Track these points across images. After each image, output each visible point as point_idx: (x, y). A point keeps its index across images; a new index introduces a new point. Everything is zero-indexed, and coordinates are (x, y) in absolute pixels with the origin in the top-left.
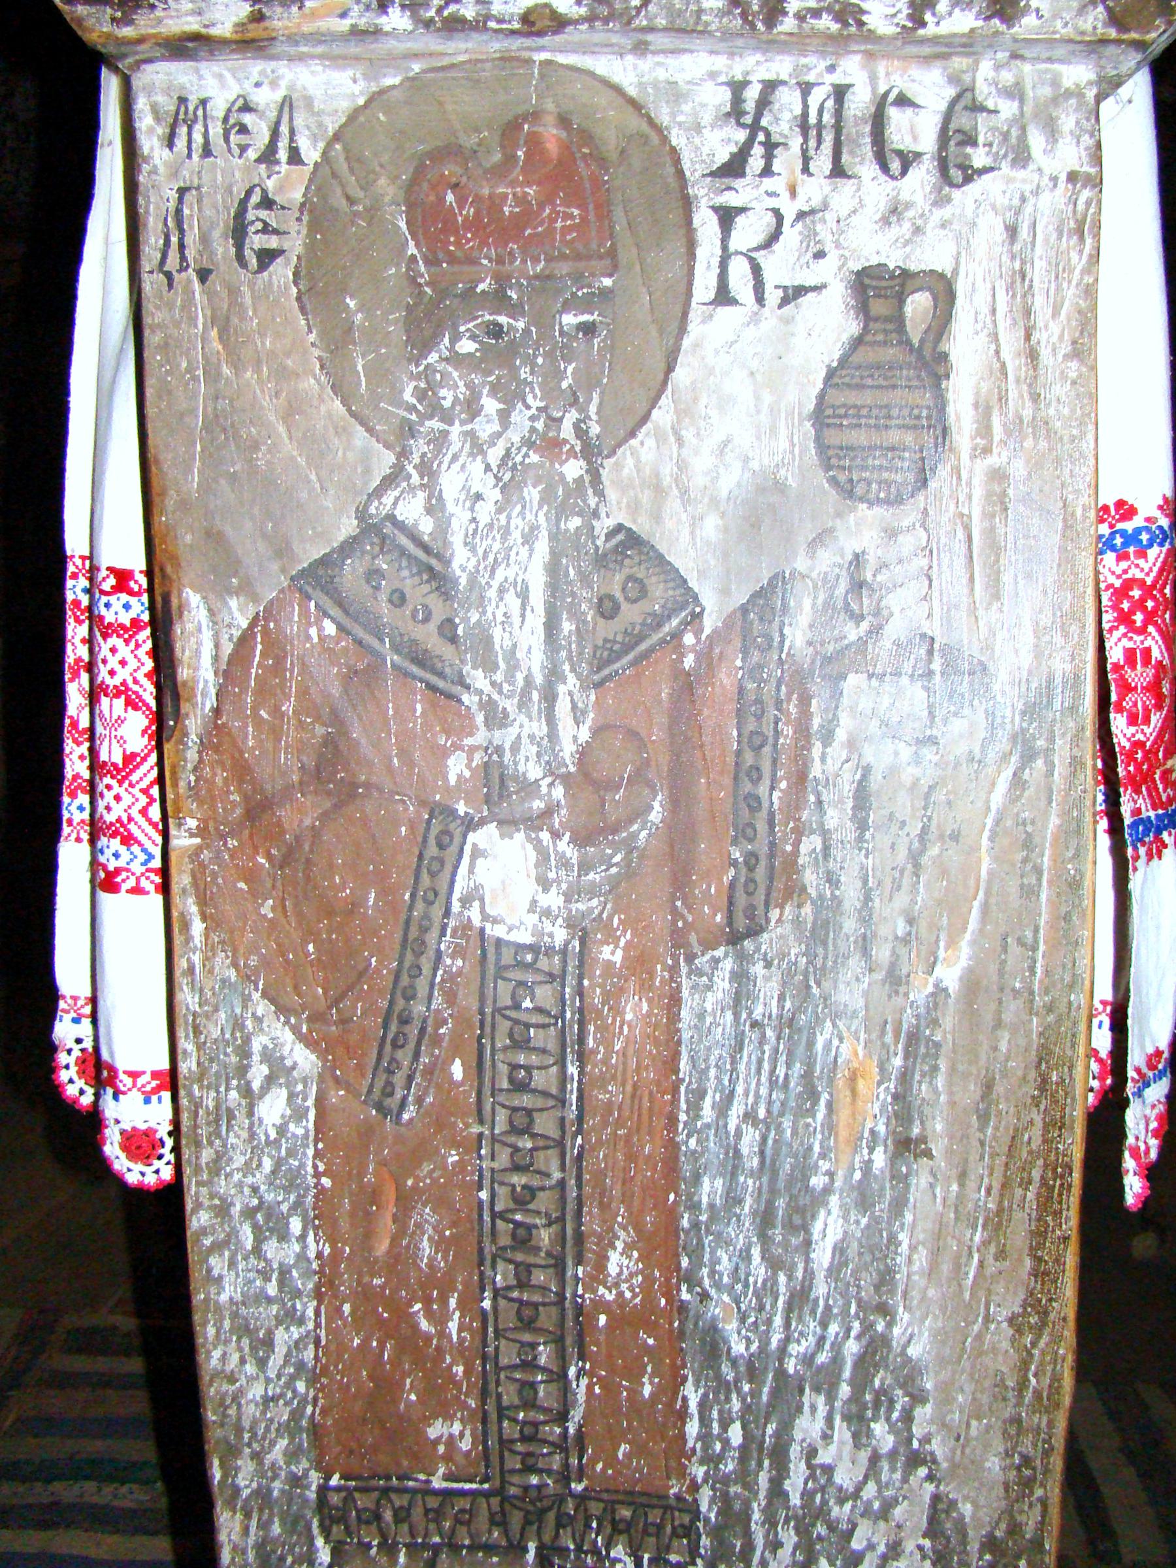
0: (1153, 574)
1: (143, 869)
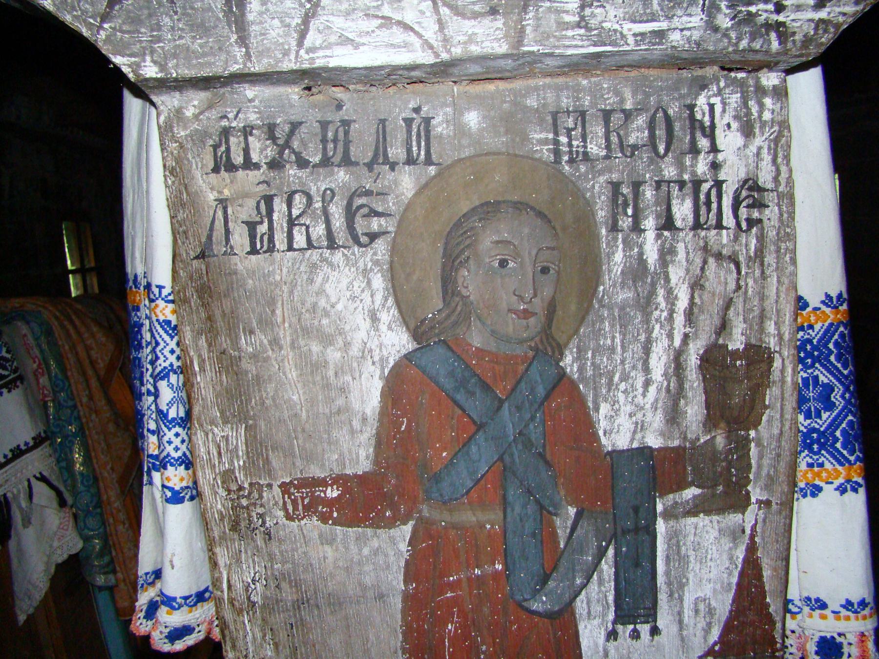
0: (824, 426)
1: (157, 302)
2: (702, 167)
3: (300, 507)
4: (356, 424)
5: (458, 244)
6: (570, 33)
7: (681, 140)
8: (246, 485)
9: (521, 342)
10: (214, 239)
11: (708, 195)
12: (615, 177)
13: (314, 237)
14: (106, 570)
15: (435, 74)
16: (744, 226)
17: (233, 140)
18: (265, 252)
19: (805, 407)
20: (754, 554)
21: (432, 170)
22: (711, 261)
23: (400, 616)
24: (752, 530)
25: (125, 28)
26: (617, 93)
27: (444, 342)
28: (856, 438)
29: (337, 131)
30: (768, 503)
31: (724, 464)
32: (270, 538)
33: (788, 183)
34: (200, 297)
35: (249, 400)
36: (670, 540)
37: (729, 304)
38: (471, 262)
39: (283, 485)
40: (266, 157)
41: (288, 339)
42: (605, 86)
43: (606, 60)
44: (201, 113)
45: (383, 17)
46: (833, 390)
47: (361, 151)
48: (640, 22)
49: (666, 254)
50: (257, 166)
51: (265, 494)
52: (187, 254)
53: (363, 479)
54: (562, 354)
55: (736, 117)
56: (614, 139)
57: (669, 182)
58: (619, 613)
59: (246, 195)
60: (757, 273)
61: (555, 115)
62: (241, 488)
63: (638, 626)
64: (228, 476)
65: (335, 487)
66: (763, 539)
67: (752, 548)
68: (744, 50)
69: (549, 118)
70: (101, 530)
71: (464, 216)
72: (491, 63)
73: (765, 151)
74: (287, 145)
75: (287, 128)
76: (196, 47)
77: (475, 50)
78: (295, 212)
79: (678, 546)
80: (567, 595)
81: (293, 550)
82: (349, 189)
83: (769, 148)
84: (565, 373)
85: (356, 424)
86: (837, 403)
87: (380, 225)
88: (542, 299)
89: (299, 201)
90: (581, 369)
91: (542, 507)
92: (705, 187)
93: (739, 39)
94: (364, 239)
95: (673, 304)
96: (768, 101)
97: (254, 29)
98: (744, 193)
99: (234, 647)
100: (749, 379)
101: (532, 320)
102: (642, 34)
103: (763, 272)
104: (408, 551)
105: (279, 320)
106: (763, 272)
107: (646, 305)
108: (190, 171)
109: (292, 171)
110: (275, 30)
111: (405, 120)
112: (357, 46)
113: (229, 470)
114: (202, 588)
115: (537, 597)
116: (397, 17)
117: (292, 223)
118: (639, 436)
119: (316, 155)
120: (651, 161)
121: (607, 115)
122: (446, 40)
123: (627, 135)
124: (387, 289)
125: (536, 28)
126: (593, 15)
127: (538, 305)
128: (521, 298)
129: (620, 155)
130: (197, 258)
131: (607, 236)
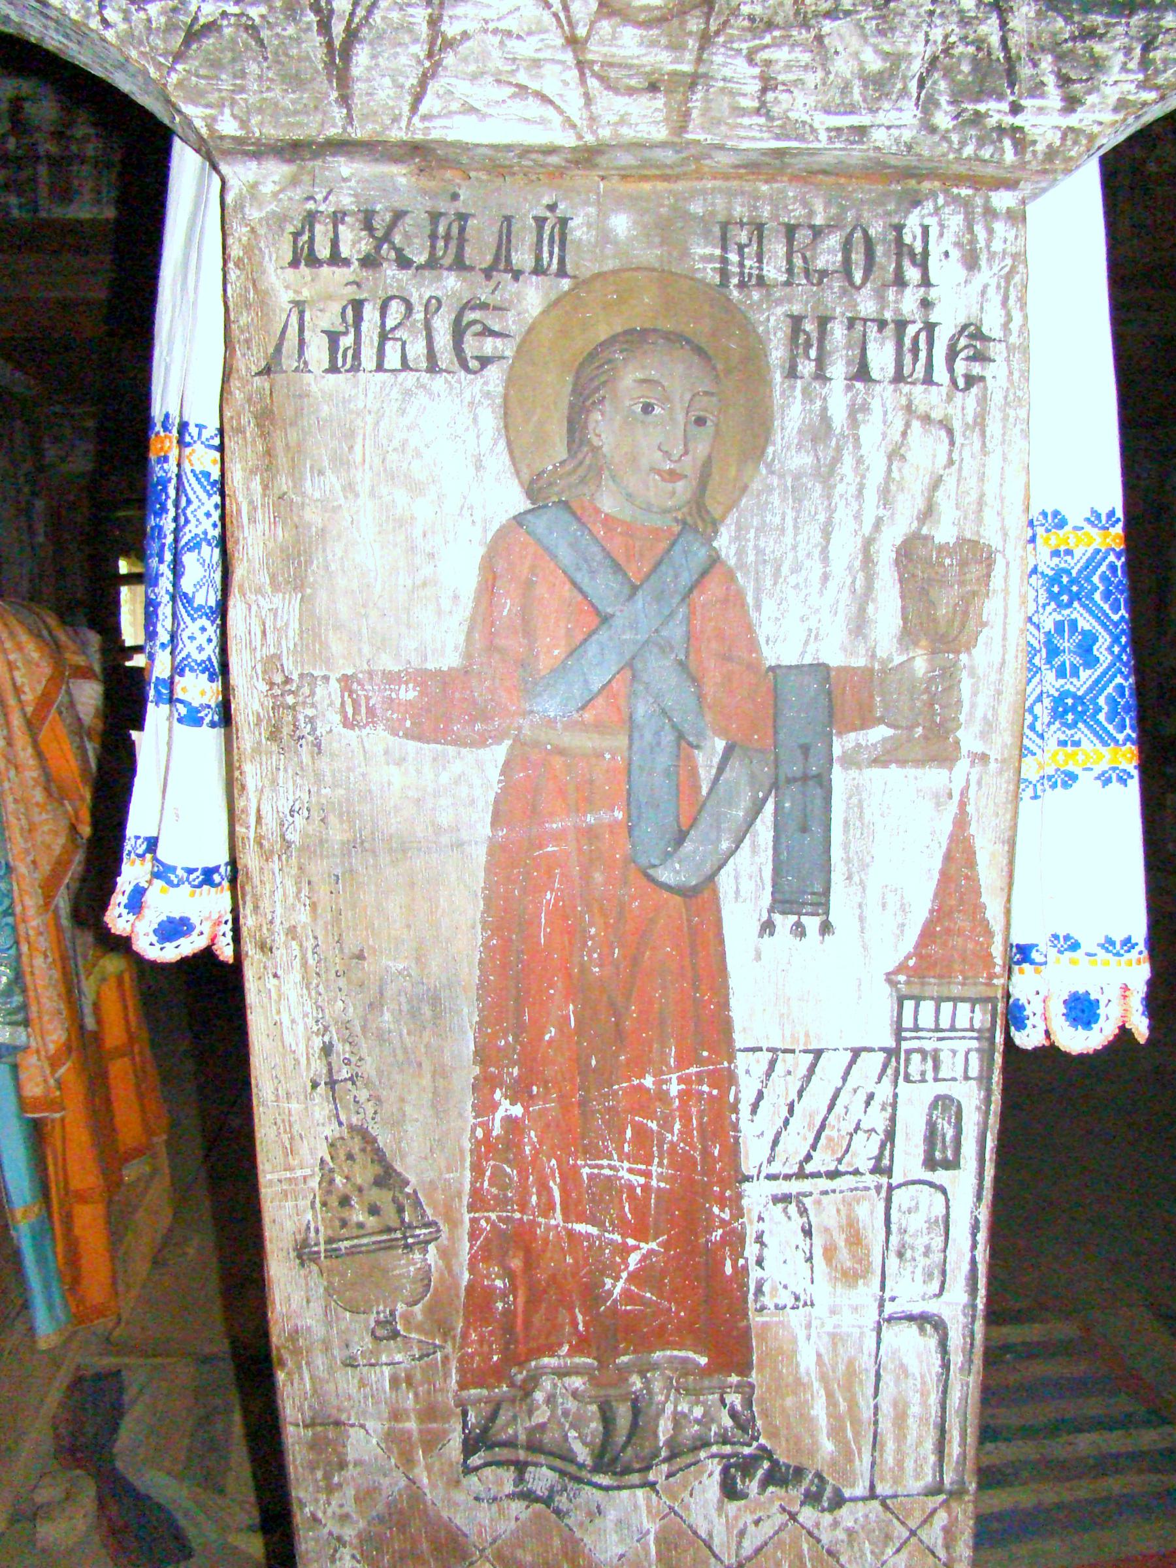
2: (909, 303)
3: (363, 710)
4: (446, 604)
5: (592, 380)
6: (746, 121)
7: (883, 268)
8: (295, 677)
9: (665, 511)
10: (284, 350)
11: (916, 339)
12: (796, 309)
13: (411, 356)
14: (14, 1018)
15: (577, 163)
16: (961, 383)
17: (318, 228)
18: (348, 371)
19: (1057, 662)
20: (964, 830)
21: (566, 284)
22: (916, 424)
23: (482, 874)
24: (962, 794)
25: (202, 72)
26: (805, 204)
27: (566, 503)
28: (1127, 709)
29: (450, 225)
30: (984, 758)
31: (925, 697)
32: (319, 753)
33: (1020, 333)
34: (258, 425)
35: (309, 562)
36: (850, 798)
37: (936, 483)
38: (607, 403)
39: (346, 680)
40: (359, 252)
41: (368, 483)
42: (791, 194)
43: (793, 161)
44: (282, 191)
45: (517, 86)
46: (1095, 640)
47: (479, 253)
48: (836, 114)
49: (856, 412)
50: (346, 262)
51: (318, 690)
52: (248, 369)
53: (444, 679)
54: (716, 532)
55: (958, 245)
56: (798, 261)
57: (865, 320)
58: (778, 896)
59: (331, 298)
60: (977, 445)
61: (725, 226)
62: (288, 680)
63: (804, 919)
64: (272, 662)
65: (411, 686)
66: (977, 810)
67: (961, 822)
68: (969, 159)
69: (717, 230)
70: (13, 951)
71: (601, 344)
72: (648, 154)
73: (991, 291)
74: (387, 238)
75: (388, 217)
76: (286, 103)
77: (627, 133)
78: (390, 324)
79: (861, 807)
80: (708, 865)
81: (349, 769)
82: (460, 298)
83: (998, 287)
84: (719, 557)
85: (446, 604)
86: (1102, 659)
87: (495, 348)
88: (694, 460)
89: (396, 310)
90: (741, 553)
91: (681, 736)
92: (911, 330)
93: (963, 143)
94: (474, 364)
95: (863, 477)
96: (999, 227)
97: (359, 87)
98: (963, 342)
99: (256, 908)
100: (962, 583)
101: (680, 485)
102: (839, 130)
103: (984, 444)
104: (499, 782)
105: (359, 459)
106: (984, 444)
107: (826, 474)
108: (261, 264)
109: (390, 271)
110: (385, 91)
111: (536, 218)
112: (483, 117)
113: (274, 655)
114: (211, 865)
115: (668, 863)
116: (534, 85)
117: (384, 337)
118: (811, 648)
119: (420, 254)
120: (844, 292)
121: (790, 231)
122: (592, 119)
123: (814, 258)
124: (498, 430)
125: (705, 112)
126: (777, 101)
127: (688, 466)
128: (667, 454)
129: (804, 281)
130: (259, 374)
131: (782, 383)
